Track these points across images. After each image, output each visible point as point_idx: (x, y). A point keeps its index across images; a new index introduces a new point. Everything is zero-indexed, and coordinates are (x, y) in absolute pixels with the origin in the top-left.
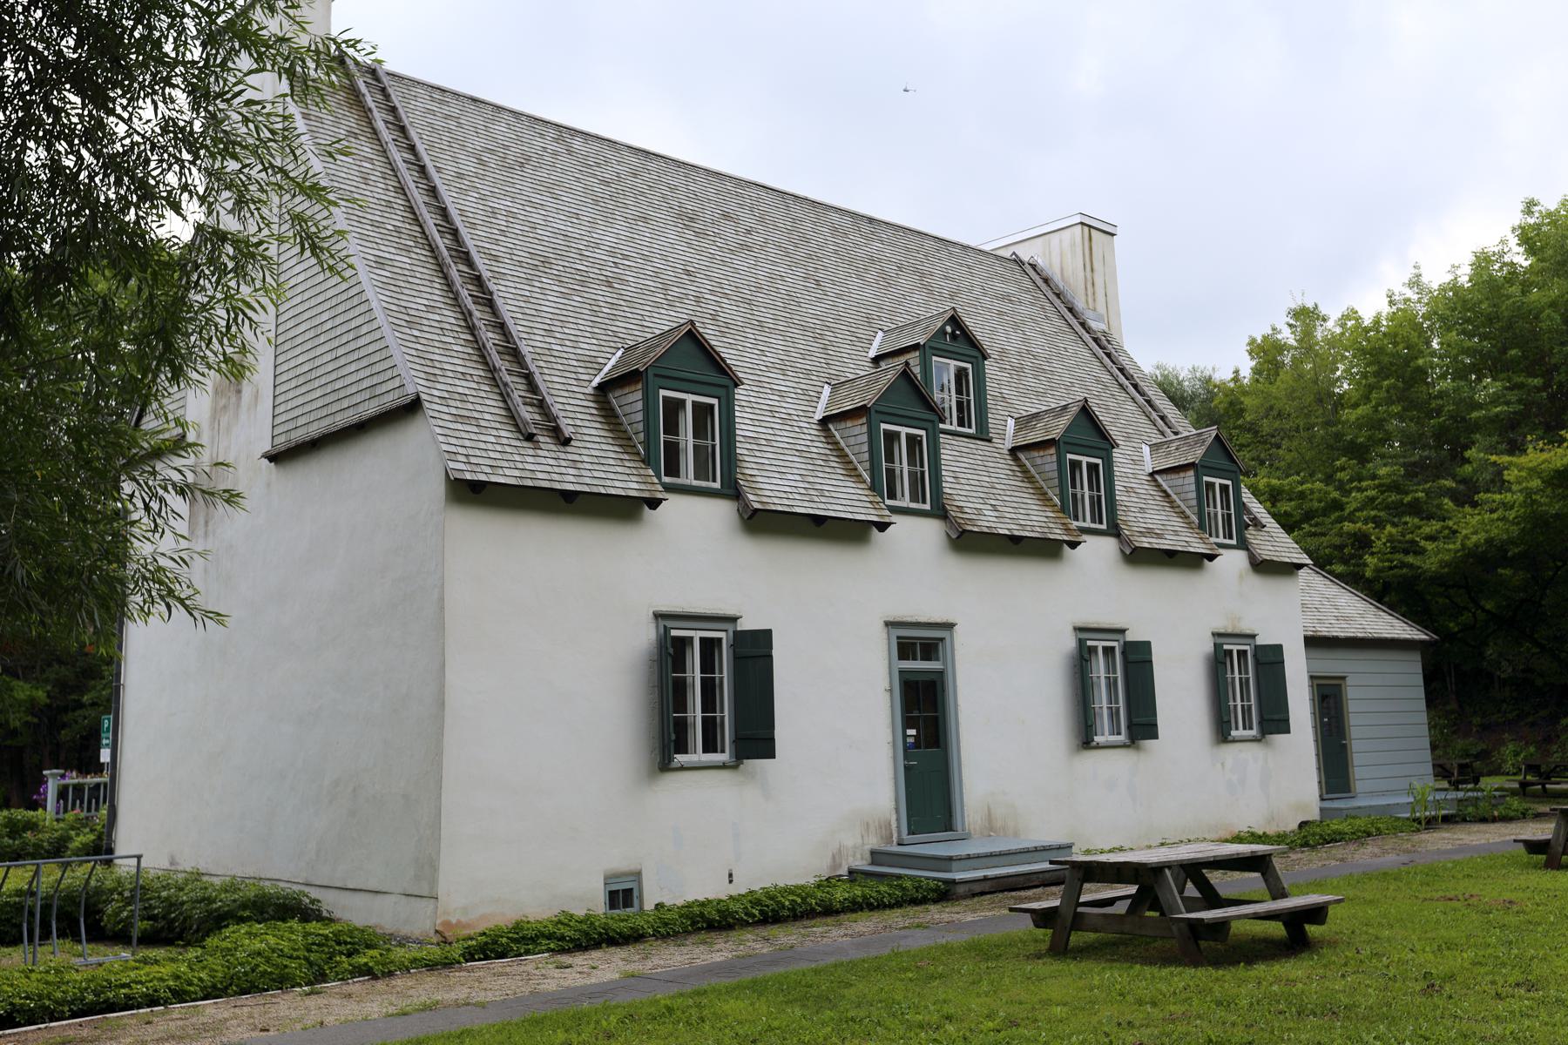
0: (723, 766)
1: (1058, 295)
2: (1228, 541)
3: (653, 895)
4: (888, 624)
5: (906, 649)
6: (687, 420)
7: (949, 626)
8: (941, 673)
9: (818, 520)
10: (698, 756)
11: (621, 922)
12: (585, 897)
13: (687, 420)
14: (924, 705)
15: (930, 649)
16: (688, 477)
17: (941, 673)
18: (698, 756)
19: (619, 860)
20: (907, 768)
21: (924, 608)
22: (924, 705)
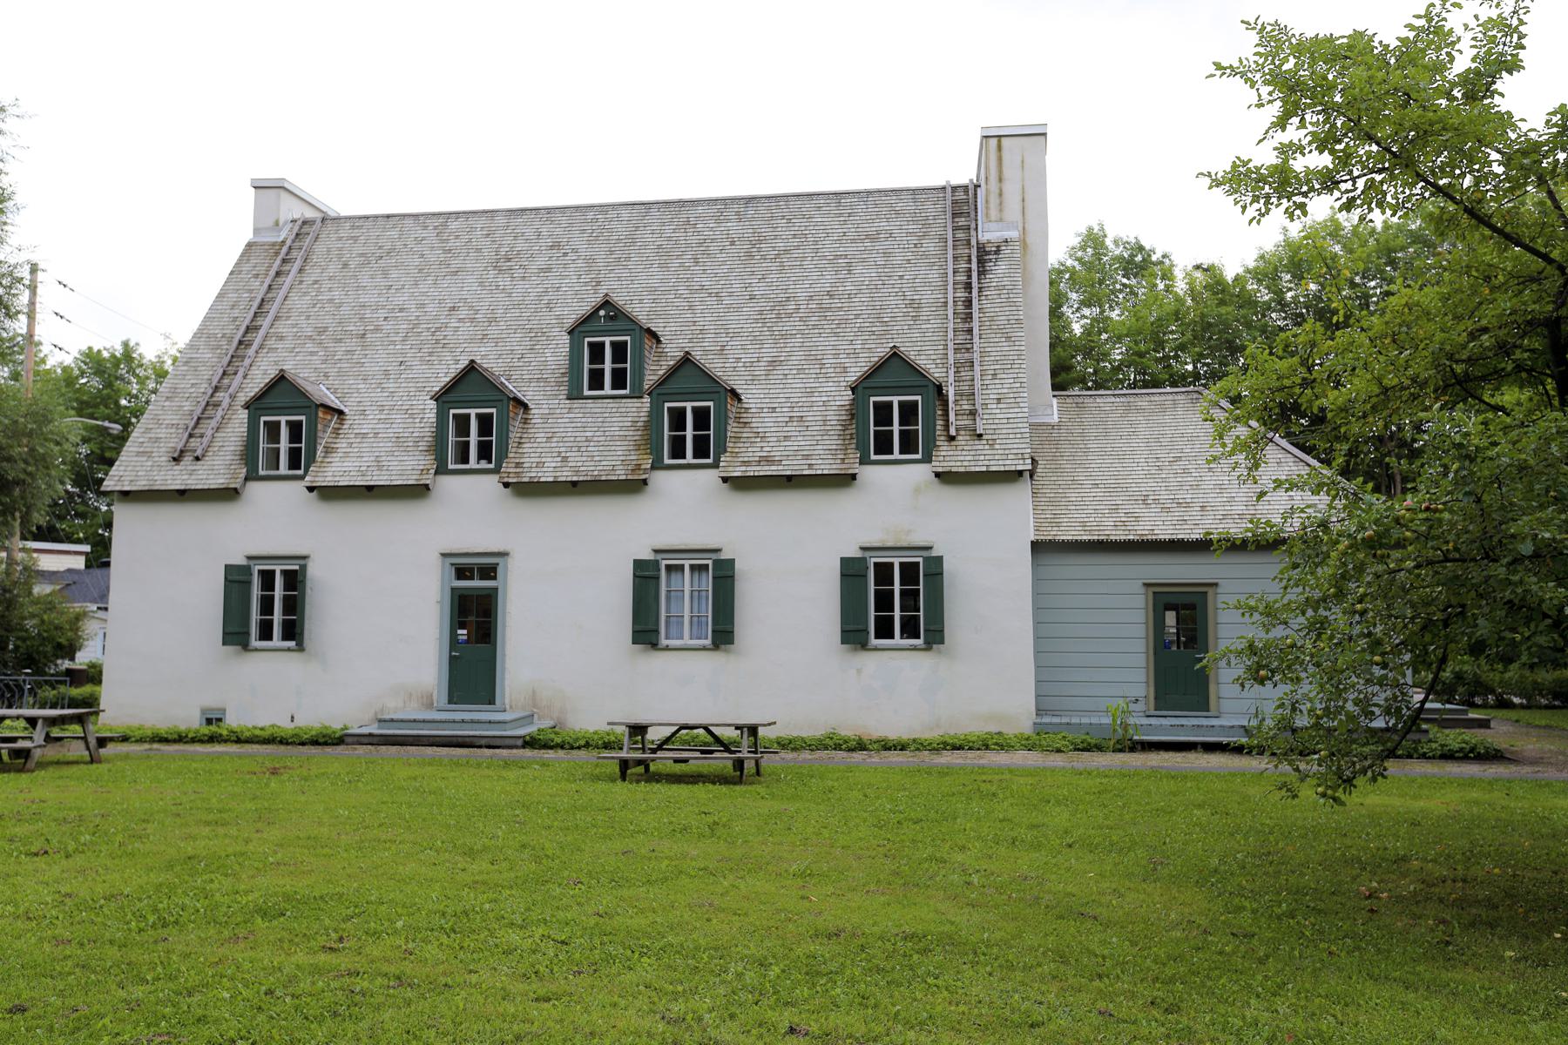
0: (704, 649)
1: (1000, 180)
2: (484, 465)
3: (233, 721)
4: (444, 555)
5: (462, 572)
6: (284, 433)
7: (504, 554)
8: (496, 589)
9: (370, 488)
10: (898, 640)
11: (213, 731)
12: (191, 720)
13: (284, 433)
14: (474, 611)
15: (489, 572)
16: (473, 463)
17: (496, 589)
18: (898, 640)
19: (211, 700)
20: (451, 657)
21: (476, 539)
22: (474, 611)
